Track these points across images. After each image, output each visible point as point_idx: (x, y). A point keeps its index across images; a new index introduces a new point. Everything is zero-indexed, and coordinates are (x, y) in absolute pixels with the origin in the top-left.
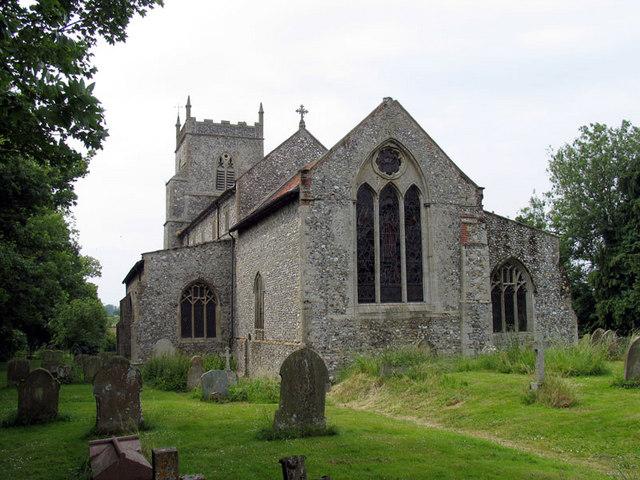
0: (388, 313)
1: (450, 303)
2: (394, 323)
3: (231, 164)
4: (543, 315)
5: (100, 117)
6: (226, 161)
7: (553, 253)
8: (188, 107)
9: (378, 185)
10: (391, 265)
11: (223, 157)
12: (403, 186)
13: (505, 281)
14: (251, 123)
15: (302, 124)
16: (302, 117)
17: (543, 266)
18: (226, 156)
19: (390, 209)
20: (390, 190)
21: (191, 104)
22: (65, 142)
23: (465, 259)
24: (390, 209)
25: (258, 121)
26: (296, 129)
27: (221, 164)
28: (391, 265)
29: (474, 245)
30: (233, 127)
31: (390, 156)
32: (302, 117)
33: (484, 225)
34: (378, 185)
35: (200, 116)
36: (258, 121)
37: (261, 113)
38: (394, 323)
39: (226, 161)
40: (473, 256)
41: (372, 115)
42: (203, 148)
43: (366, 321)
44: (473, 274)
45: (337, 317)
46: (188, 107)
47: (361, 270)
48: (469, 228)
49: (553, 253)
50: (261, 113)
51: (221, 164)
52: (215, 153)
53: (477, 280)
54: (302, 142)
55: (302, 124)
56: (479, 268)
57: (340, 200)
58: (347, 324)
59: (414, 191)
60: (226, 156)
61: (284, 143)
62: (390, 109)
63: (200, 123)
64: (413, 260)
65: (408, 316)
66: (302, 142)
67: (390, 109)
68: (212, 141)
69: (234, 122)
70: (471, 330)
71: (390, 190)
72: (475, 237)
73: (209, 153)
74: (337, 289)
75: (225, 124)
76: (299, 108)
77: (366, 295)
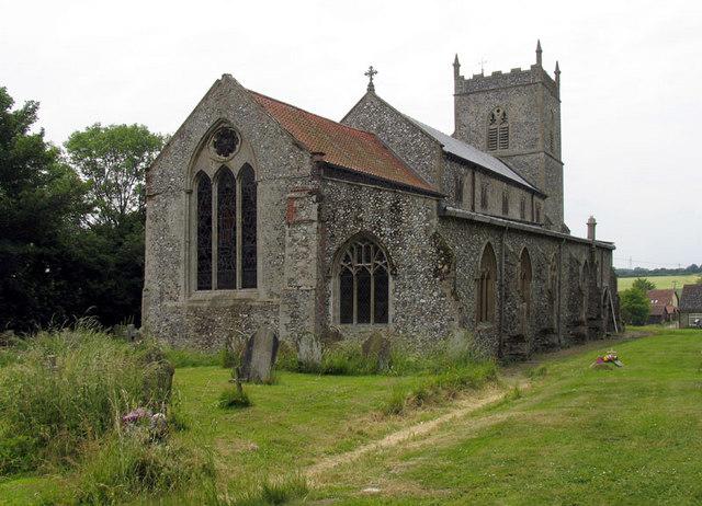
0: (214, 300)
1: (273, 290)
2: (218, 310)
3: (504, 119)
4: (404, 304)
5: (145, 132)
6: (498, 117)
7: (425, 222)
8: (457, 65)
9: (212, 170)
10: (227, 251)
11: (495, 113)
12: (235, 165)
13: (359, 261)
14: (526, 67)
15: (371, 87)
16: (371, 79)
17: (408, 239)
18: (498, 111)
19: (227, 194)
20: (224, 173)
21: (460, 61)
22: (461, 74)
23: (289, 240)
24: (227, 194)
25: (535, 62)
26: (364, 91)
27: (493, 120)
28: (227, 251)
29: (299, 223)
30: (505, 76)
31: (225, 139)
32: (371, 79)
33: (314, 198)
34: (212, 170)
35: (468, 73)
36: (535, 62)
37: (539, 52)
38: (218, 310)
39: (498, 117)
40: (298, 236)
41: (206, 98)
42: (472, 108)
43: (191, 308)
44: (296, 256)
45: (170, 304)
46: (457, 65)
47: (201, 258)
48: (296, 204)
49: (425, 222)
50: (539, 52)
51: (493, 120)
52: (485, 111)
53: (301, 264)
54: (369, 107)
55: (371, 87)
56: (304, 249)
57: (171, 191)
58: (176, 311)
59: (247, 170)
60: (498, 111)
61: (349, 113)
62: (225, 88)
63: (469, 81)
64: (249, 244)
65: (231, 303)
66: (369, 107)
67: (225, 88)
68: (482, 98)
69: (506, 70)
70: (288, 320)
71: (224, 173)
72: (303, 213)
73: (486, 104)
74: (172, 277)
75: (497, 75)
76: (374, 69)
77: (204, 284)
